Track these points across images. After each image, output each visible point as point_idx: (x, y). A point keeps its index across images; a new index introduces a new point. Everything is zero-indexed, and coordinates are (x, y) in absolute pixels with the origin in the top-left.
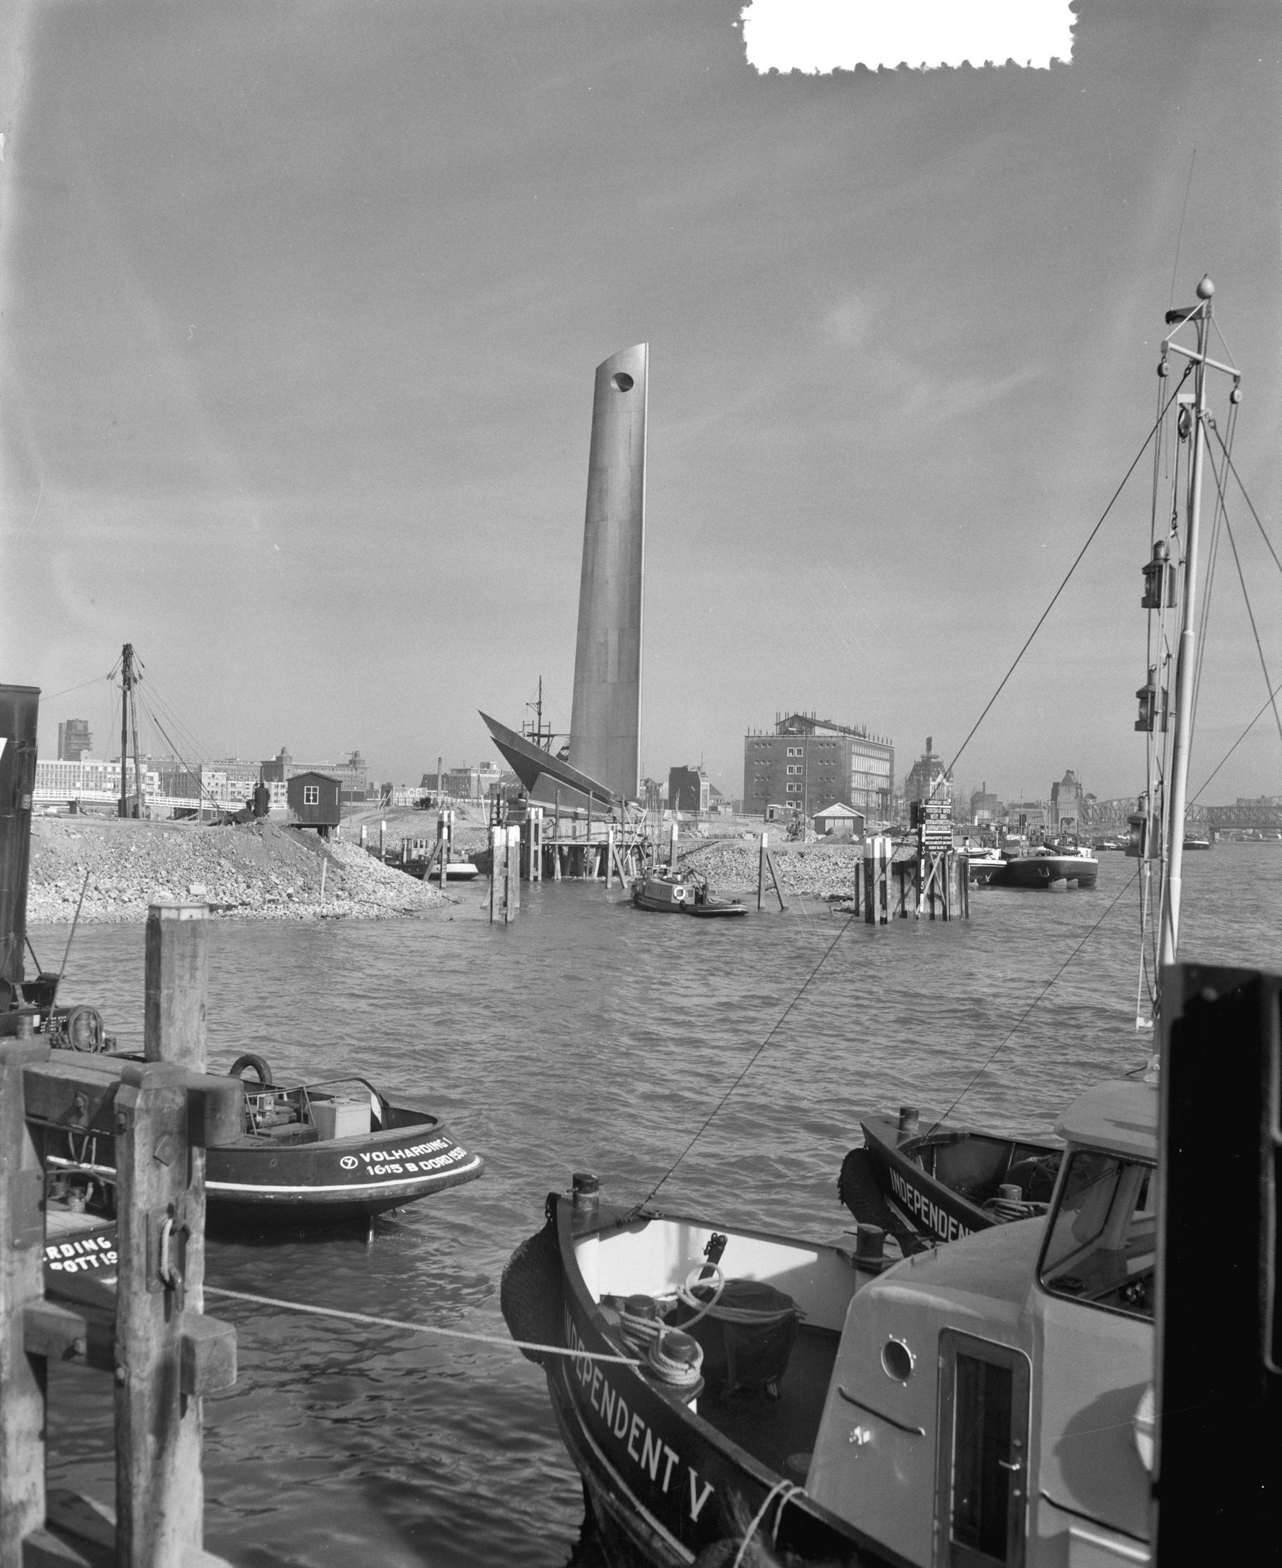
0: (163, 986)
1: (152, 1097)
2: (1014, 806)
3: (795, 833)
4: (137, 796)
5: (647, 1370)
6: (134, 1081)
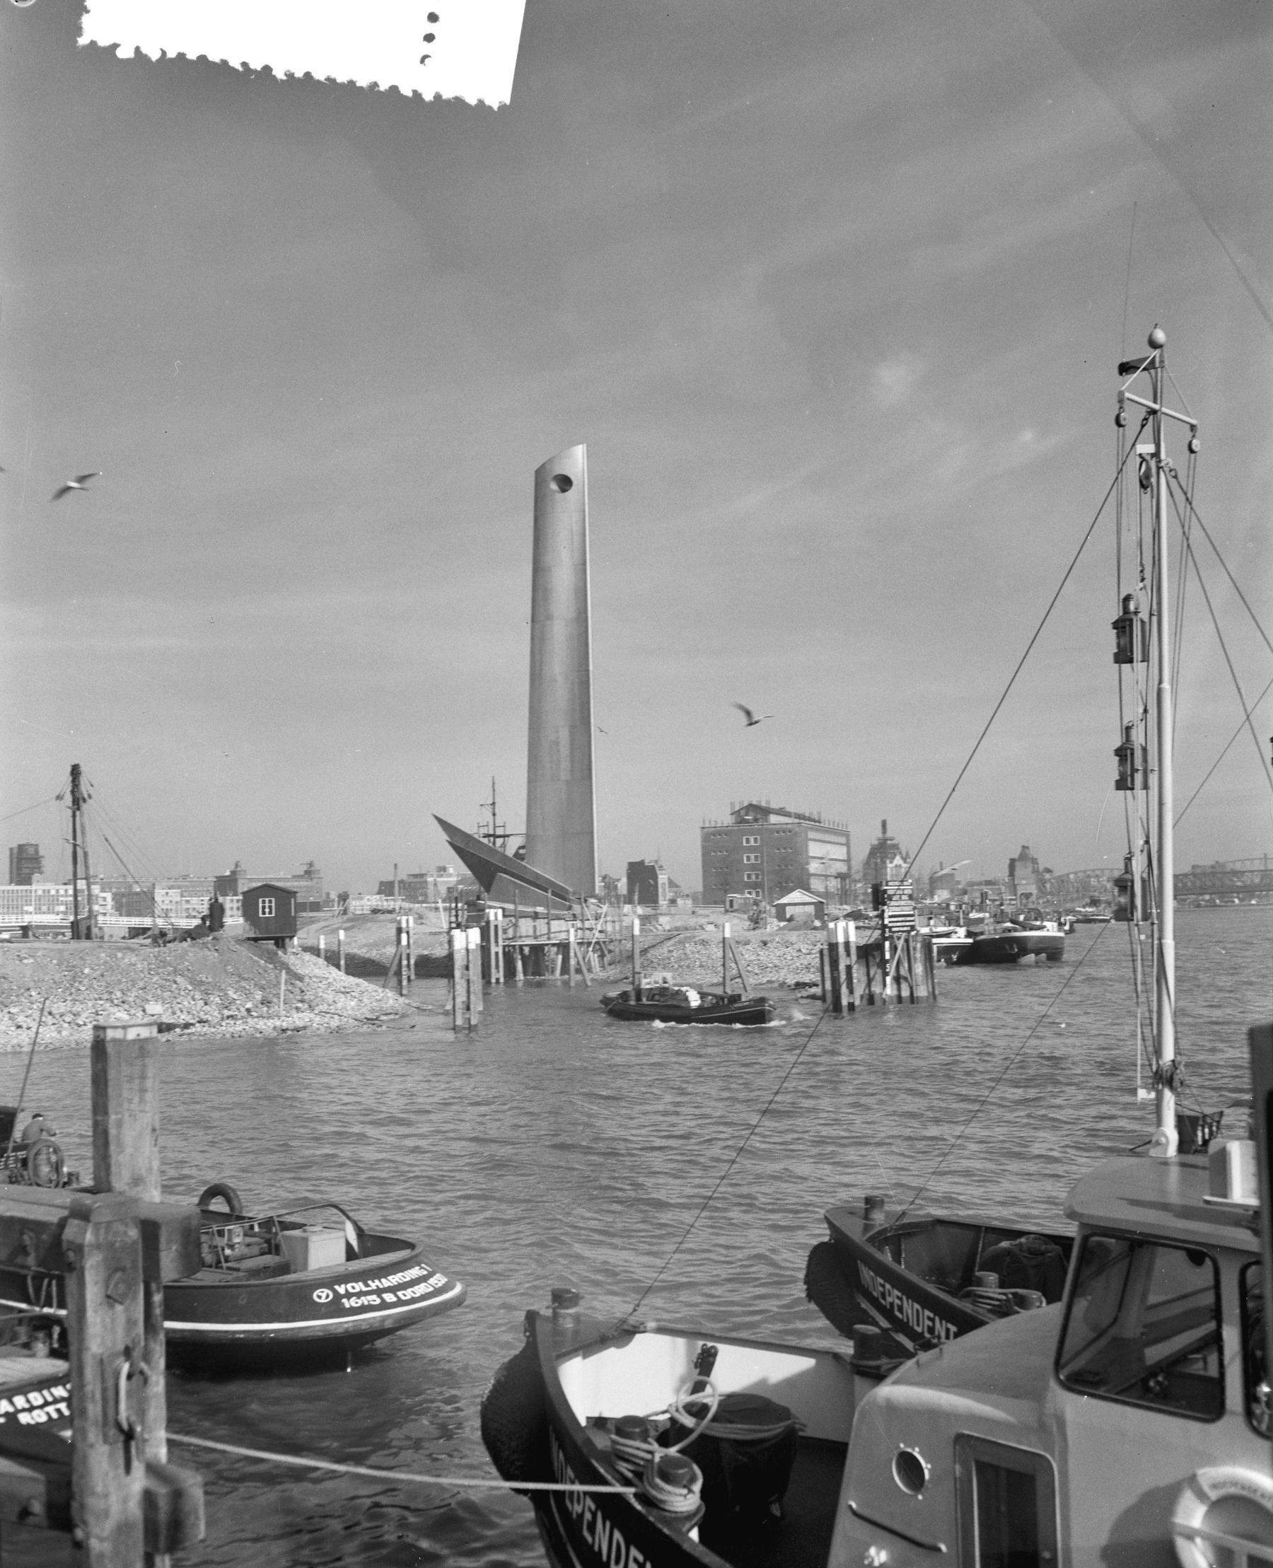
0: (111, 1111)
1: (102, 1231)
2: (972, 884)
3: (756, 922)
4: (89, 918)
5: (643, 1497)
6: (82, 1214)
